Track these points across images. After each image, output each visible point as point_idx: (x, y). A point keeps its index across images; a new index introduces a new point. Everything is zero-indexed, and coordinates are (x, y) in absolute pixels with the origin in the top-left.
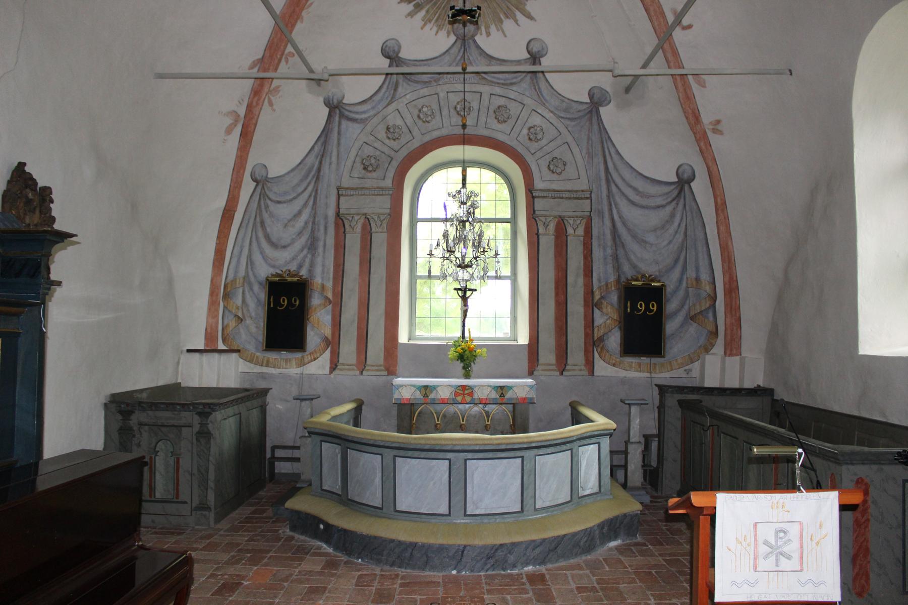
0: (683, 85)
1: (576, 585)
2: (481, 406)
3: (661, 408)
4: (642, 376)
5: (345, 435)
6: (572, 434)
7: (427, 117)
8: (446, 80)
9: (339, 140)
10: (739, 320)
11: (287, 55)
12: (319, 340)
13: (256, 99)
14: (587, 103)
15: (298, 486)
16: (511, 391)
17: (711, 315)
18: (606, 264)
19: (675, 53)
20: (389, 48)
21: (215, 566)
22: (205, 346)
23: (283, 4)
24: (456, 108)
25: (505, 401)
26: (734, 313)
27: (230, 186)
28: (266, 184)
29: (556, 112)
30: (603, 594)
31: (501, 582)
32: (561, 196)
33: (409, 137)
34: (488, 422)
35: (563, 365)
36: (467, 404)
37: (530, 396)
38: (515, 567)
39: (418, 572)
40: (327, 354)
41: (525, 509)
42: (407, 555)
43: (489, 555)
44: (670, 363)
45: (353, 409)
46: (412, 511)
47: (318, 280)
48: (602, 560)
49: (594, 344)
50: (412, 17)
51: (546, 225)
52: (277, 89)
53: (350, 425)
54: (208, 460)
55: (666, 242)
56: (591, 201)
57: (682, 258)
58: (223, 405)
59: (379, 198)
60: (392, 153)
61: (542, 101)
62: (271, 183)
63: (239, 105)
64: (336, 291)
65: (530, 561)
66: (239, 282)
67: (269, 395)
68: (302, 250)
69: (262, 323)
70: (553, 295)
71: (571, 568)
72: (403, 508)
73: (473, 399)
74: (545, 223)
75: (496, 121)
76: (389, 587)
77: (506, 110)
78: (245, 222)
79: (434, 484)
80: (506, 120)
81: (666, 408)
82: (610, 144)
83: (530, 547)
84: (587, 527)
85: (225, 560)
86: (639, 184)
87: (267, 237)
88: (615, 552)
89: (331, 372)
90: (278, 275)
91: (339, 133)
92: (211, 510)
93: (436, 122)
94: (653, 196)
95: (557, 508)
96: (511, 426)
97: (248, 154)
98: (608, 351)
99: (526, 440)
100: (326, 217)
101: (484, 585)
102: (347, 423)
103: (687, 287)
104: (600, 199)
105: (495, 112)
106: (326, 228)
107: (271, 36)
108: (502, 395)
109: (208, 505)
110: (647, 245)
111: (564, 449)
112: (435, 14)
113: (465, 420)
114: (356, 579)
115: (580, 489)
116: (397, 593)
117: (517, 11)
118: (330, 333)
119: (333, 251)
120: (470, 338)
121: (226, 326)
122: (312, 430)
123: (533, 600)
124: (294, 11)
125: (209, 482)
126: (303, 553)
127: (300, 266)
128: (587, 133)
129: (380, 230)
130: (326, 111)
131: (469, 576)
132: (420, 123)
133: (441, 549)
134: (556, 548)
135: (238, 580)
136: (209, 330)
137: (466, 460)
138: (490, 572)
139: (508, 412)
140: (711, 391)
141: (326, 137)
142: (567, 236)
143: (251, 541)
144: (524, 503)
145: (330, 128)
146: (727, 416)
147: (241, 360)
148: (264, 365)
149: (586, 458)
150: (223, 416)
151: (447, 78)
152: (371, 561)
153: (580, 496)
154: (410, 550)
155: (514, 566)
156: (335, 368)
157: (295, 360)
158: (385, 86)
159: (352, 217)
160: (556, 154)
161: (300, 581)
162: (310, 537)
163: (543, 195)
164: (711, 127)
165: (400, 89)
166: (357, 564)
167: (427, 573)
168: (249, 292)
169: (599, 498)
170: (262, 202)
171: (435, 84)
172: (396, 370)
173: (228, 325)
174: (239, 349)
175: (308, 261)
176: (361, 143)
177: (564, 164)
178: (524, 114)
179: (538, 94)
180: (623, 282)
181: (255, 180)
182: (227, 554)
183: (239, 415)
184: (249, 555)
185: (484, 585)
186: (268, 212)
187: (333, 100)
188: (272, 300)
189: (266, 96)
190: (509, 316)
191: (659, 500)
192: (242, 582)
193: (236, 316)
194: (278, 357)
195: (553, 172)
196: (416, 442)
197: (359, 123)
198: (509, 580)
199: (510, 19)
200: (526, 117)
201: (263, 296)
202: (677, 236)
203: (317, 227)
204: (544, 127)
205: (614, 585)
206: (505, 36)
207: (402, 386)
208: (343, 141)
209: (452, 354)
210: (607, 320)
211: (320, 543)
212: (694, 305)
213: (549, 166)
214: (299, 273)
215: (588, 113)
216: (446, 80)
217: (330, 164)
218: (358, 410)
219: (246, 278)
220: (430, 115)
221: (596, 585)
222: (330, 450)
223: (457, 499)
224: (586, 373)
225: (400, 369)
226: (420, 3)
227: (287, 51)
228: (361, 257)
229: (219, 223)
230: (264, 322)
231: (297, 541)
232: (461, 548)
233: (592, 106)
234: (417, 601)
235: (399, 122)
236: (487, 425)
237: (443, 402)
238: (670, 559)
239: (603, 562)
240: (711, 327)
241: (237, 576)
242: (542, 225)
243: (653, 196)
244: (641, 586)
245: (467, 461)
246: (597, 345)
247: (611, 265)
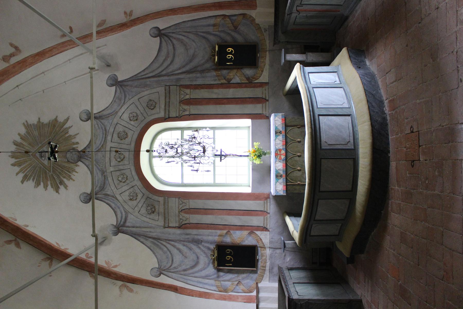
9: (137, 227)
17: (234, 18)
37: (281, 116)
40: (258, 233)
47: (216, 239)
57: (204, 35)
68: (200, 248)
70: (223, 105)
73: (283, 149)
89: (268, 231)
90: (213, 263)
93: (127, 172)
98: (255, 75)
106: (187, 234)
119: (200, 230)
127: (209, 248)
132: (128, 182)
158: (107, 201)
160: (145, 105)
170: (172, 271)
175: (207, 245)
178: (123, 123)
181: (160, 275)
193: (237, 285)
195: (155, 107)
208: (138, 225)
209: (258, 162)
217: (151, 232)
224: (267, 87)
235: (127, 193)
240: (241, 17)
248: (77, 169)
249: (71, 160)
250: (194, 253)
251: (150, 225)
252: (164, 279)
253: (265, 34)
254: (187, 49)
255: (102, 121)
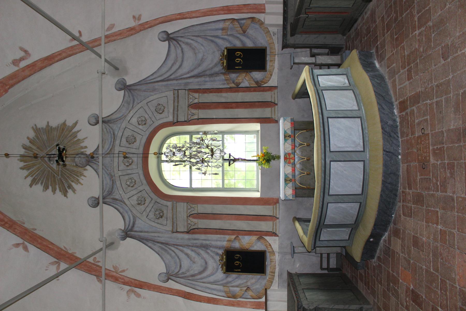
0: (113, 36)
1: (406, 81)
2: (296, 148)
3: (295, 46)
4: (277, 59)
5: (316, 227)
6: (313, 89)
7: (133, 182)
8: (112, 171)
9: (145, 232)
10: (245, 5)
11: (95, 262)
12: (259, 243)
13: (120, 280)
14: (124, 92)
15: (344, 254)
16: (287, 131)
17: (243, 22)
18: (214, 81)
19: (95, 40)
20: (93, 203)
21: (400, 306)
22: (263, 309)
23: (64, 264)
24: (128, 166)
25: (293, 135)
26: (241, 8)
27: (171, 295)
28: (170, 274)
29: (130, 109)
30: (412, 64)
31: (406, 127)
32: (177, 106)
33: (144, 192)
34: (305, 144)
35: (272, 104)
36: (295, 157)
38: (395, 120)
39: (400, 179)
40: (267, 238)
41: (359, 116)
42: (389, 186)
43: (389, 136)
44: (269, 44)
45: (299, 223)
46: (362, 184)
47: (225, 244)
48: (388, 69)
49: (260, 86)
50: (75, 190)
51: (193, 115)
52: (115, 267)
53: (309, 224)
54: (332, 309)
55: (202, 48)
56: (179, 89)
58: (298, 300)
59: (178, 209)
60: (153, 201)
61: (124, 117)
62: (169, 271)
63: (123, 290)
64: (231, 233)
65: (391, 111)
66: (226, 289)
67: (291, 272)
69: (250, 276)
71: (394, 86)
72: (360, 189)
73: (292, 153)
74: (192, 115)
75: (135, 143)
76: (412, 196)
77: (129, 137)
78: (191, 286)
79: (345, 170)
80: (134, 138)
81: (295, 43)
82: (148, 79)
83: (383, 111)
84: (369, 79)
85: (395, 300)
86: (170, 63)
87: (201, 273)
88: (383, 63)
89: (278, 236)
90: (222, 267)
91: (141, 232)
92: (362, 307)
93: (135, 177)
94: (177, 55)
95: (357, 98)
96: (307, 131)
97: (152, 284)
98: (263, 79)
99: (317, 116)
100: (189, 239)
101: (409, 138)
102: (308, 226)
103: (227, 35)
104: (178, 84)
105: (130, 144)
106: (195, 239)
107: (83, 271)
108: (290, 136)
109: (359, 309)
110: (204, 58)
111: (322, 94)
112: (74, 177)
113: (304, 158)
114: (406, 217)
115: (345, 85)
116: (416, 191)
117: (72, 131)
118: (255, 236)
119: (209, 235)
120: (257, 156)
121: (252, 297)
122: (313, 246)
123: (418, 106)
124: (68, 258)
125: (345, 308)
126: (389, 251)
127: (217, 254)
128: (141, 92)
129: (196, 208)
130: (128, 239)
131: (402, 148)
132: (136, 186)
133: (385, 165)
134: (383, 96)
135: (410, 292)
136: (254, 307)
137: (330, 152)
138: (399, 135)
139: (299, 133)
140: (285, 19)
141: (143, 239)
142: (199, 103)
143: (382, 283)
144: (355, 116)
145: (138, 237)
146: (299, 6)
147: (271, 288)
148: (273, 274)
149: (327, 82)
150: (305, 300)
151: (111, 171)
152: (394, 208)
153: (349, 85)
154: (387, 184)
155: (395, 121)
156: (275, 233)
157: (271, 256)
158: (115, 206)
159: (189, 224)
160: (153, 109)
161: (409, 253)
162: (378, 247)
163: (176, 117)
164: (137, 21)
165: (117, 197)
166: (396, 217)
167: (401, 173)
168: (232, 284)
169: (350, 75)
170: (180, 276)
171: (114, 177)
172: (276, 198)
173: (251, 296)
174: (265, 289)
175: (214, 250)
176: (147, 219)
177: (159, 105)
179: (120, 119)
180: (224, 71)
182: (391, 297)
183: (304, 290)
184: (391, 284)
185: (409, 138)
186: (186, 272)
187: (122, 235)
188: (236, 270)
189: (118, 274)
190: (244, 135)
191: (348, 46)
192: (411, 289)
193: (246, 291)
194: (269, 266)
195: (163, 111)
196: (320, 182)
197: (135, 221)
198: (404, 123)
199: (77, 135)
200: (133, 126)
201: (234, 275)
202: (198, 41)
203: (194, 244)
204: (138, 116)
205: (406, 58)
206: (87, 138)
207: (285, 194)
208: (146, 230)
209: (266, 166)
210: (246, 79)
211: (382, 240)
212: (237, 31)
213: (160, 113)
214: (220, 255)
215: (130, 92)
216: (112, 171)
217: (159, 237)
218: (299, 220)
219: (224, 285)
220: (132, 180)
221: (406, 69)
222: (325, 235)
223: (354, 157)
224: (276, 91)
225: (275, 196)
226: (68, 185)
227: (93, 262)
228: (211, 219)
229: (192, 301)
230: (249, 275)
231: (381, 255)
232: (385, 153)
233: (126, 89)
234: (421, 178)
235: (135, 198)
236: (307, 145)
237: (294, 170)
238: (386, 29)
239: (389, 69)
240: (249, 21)
241: (407, 292)
242: (193, 117)
243: (177, 55)
244: (406, 42)
245: (331, 150)
246: (260, 85)
247: (215, 78)
248: (85, 173)
249: (79, 165)
250: (203, 258)
251: (158, 230)
252: (171, 284)
253: (273, 37)
254: (196, 54)
255: (110, 125)
